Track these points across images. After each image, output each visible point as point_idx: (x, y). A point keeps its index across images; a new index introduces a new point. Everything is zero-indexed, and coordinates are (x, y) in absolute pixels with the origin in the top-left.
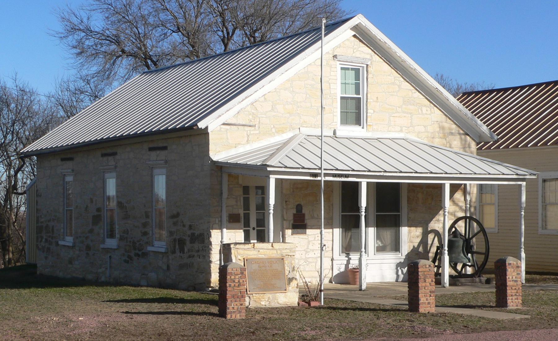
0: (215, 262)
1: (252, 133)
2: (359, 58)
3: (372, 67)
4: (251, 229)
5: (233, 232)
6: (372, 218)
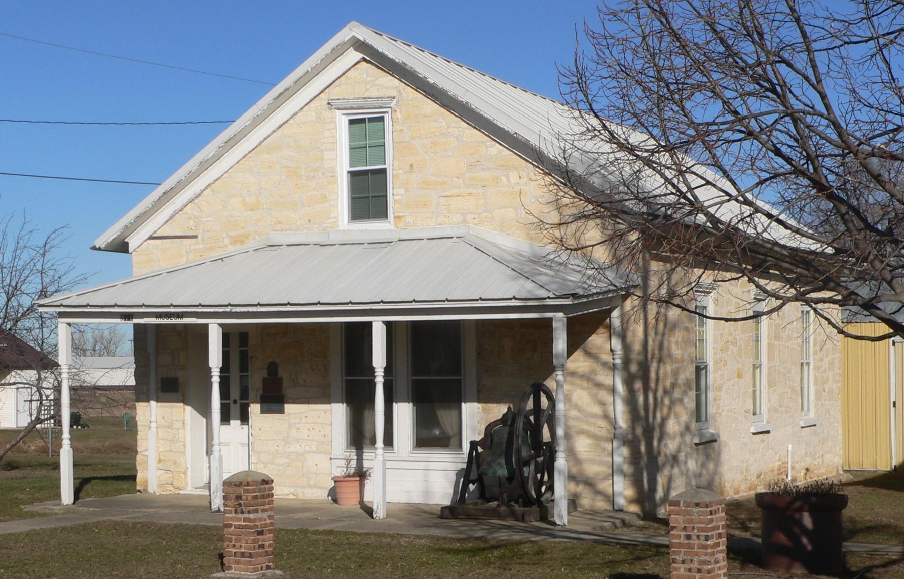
0: (143, 453)
1: (192, 248)
2: (369, 98)
3: (398, 111)
4: (231, 402)
5: (167, 406)
6: (403, 382)
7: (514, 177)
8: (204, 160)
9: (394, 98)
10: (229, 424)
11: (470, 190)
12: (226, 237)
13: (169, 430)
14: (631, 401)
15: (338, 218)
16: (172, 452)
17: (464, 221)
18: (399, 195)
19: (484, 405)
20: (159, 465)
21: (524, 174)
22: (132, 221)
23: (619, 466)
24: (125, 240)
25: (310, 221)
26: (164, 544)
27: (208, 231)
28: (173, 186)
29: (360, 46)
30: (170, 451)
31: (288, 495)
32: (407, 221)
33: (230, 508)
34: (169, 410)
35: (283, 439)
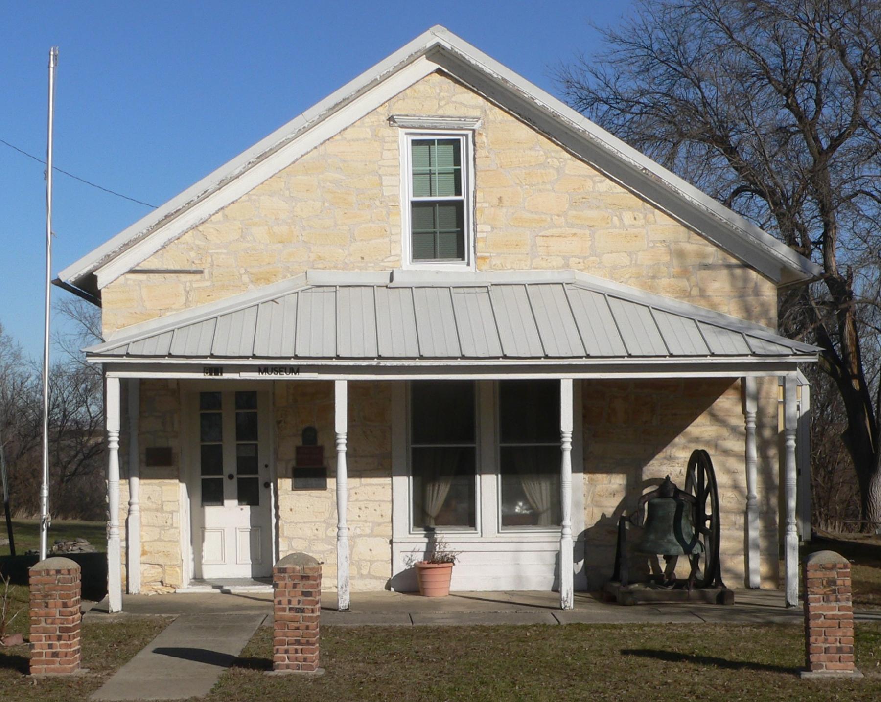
1: (194, 286)
5: (155, 484)
7: (628, 218)
8: (226, 177)
9: (479, 119)
10: (222, 504)
11: (574, 231)
12: (245, 274)
13: (159, 514)
14: (765, 471)
15: (400, 256)
16: (163, 541)
17: (567, 266)
18: (483, 232)
19: (590, 475)
20: (144, 559)
21: (640, 215)
22: (117, 249)
23: (755, 540)
24: (94, 273)
25: (363, 258)
26: (740, 645)
27: (218, 266)
28: (181, 207)
29: (437, 53)
30: (160, 540)
31: (330, 588)
32: (494, 263)
33: (817, 596)
34: (158, 488)
35: (324, 521)
